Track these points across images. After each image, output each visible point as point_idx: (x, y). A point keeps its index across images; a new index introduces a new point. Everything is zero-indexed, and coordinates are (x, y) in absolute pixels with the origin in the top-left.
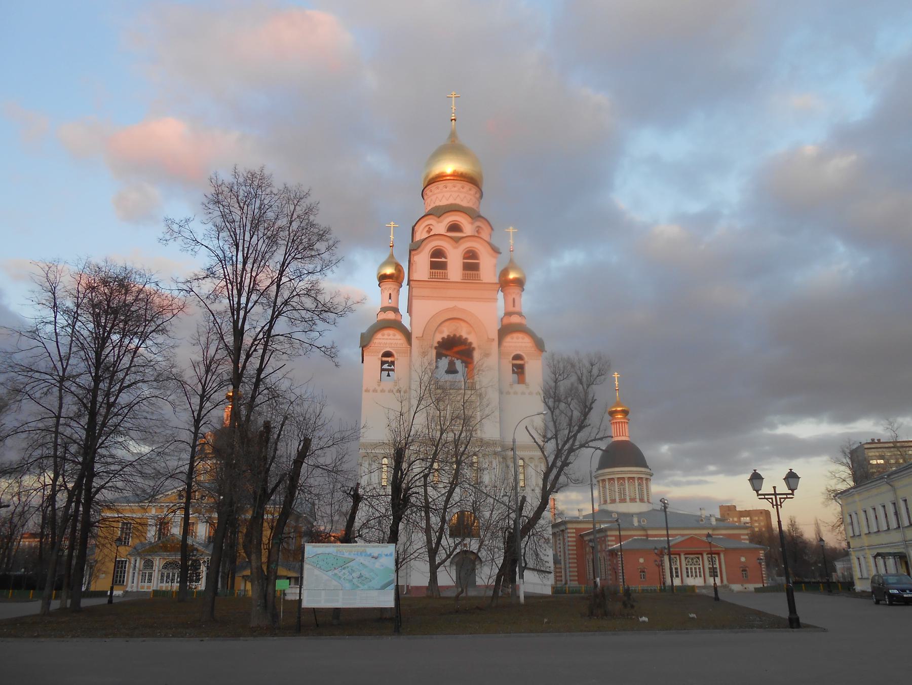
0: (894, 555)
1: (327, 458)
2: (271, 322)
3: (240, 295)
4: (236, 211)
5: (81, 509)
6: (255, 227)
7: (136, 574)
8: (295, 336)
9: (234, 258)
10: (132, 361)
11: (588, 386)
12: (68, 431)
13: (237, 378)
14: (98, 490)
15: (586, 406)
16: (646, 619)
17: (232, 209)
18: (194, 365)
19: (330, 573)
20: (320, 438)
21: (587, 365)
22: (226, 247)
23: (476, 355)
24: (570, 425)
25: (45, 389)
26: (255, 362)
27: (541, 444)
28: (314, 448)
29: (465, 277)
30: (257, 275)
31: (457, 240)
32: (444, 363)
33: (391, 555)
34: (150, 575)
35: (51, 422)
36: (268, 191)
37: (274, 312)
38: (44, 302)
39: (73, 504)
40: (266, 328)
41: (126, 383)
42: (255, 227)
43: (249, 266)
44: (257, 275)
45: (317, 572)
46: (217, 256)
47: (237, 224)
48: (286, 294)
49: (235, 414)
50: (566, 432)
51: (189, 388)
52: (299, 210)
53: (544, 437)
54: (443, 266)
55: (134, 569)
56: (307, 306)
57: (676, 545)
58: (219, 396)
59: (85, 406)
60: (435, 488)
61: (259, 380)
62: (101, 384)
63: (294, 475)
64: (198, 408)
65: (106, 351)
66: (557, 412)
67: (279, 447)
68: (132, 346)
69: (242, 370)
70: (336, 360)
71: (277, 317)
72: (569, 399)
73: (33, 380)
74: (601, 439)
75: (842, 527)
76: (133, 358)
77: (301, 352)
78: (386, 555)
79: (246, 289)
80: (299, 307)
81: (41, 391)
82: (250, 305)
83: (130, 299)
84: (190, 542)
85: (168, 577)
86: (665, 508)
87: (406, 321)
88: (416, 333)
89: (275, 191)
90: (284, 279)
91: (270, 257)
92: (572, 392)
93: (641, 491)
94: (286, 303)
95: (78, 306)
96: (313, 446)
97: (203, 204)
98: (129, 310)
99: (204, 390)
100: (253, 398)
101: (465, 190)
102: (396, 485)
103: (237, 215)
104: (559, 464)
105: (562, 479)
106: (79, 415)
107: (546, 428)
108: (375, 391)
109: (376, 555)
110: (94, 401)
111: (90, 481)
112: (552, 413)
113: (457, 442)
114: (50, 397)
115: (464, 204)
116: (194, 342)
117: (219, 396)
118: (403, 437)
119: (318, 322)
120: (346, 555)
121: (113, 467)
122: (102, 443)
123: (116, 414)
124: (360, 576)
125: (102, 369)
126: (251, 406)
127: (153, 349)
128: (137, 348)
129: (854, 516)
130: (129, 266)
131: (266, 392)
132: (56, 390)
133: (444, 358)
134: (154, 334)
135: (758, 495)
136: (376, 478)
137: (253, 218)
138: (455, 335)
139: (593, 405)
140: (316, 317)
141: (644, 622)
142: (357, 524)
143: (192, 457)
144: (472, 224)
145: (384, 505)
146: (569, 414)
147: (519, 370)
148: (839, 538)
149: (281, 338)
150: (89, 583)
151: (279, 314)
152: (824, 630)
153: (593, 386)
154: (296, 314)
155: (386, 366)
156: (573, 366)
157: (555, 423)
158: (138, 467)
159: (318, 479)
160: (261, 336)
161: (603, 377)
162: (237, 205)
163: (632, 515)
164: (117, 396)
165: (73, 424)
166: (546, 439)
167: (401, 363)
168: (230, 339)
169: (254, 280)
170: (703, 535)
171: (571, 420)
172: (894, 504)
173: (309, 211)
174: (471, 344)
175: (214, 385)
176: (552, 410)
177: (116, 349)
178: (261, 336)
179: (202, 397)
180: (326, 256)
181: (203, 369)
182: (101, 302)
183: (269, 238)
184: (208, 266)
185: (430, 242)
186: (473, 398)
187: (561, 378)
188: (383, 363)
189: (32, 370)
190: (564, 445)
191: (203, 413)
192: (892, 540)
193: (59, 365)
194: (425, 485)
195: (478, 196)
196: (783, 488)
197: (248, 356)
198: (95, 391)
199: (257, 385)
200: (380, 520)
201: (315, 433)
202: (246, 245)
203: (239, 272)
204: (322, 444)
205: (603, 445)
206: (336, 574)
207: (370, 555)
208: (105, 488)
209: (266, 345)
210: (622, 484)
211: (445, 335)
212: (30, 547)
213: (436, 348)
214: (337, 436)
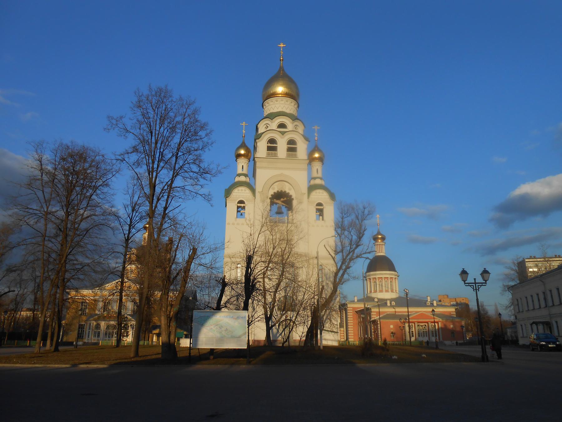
0: (543, 323)
1: (207, 259)
2: (172, 179)
3: (153, 163)
4: (150, 111)
7: (90, 333)
9: (150, 141)
12: (50, 245)
13: (151, 214)
14: (69, 280)
15: (360, 233)
16: (396, 357)
17: (148, 111)
20: (202, 248)
21: (361, 208)
22: (145, 134)
23: (295, 203)
24: (351, 244)
25: (36, 220)
26: (162, 203)
27: (334, 255)
28: (199, 254)
29: (288, 156)
30: (164, 151)
31: (283, 133)
36: (170, 99)
37: (174, 173)
38: (35, 167)
40: (169, 183)
41: (85, 215)
43: (159, 145)
44: (164, 151)
46: (140, 139)
47: (151, 120)
48: (181, 162)
49: (151, 235)
50: (349, 248)
51: (122, 220)
52: (189, 112)
53: (335, 251)
55: (90, 329)
56: (193, 170)
57: (412, 318)
58: (140, 225)
60: (270, 279)
61: (165, 215)
62: (70, 217)
63: (187, 270)
65: (73, 197)
66: (343, 236)
67: (177, 253)
68: (88, 194)
69: (155, 209)
70: (211, 202)
71: (176, 177)
72: (350, 229)
74: (369, 253)
75: (512, 307)
77: (190, 197)
79: (157, 159)
80: (188, 170)
81: (33, 221)
82: (159, 169)
83: (87, 165)
84: (123, 312)
85: (109, 334)
86: (407, 295)
89: (174, 100)
90: (180, 154)
91: (171, 140)
92: (352, 224)
93: (392, 285)
95: (55, 169)
96: (198, 253)
97: (130, 107)
98: (86, 173)
100: (162, 225)
101: (288, 103)
102: (248, 276)
103: (151, 114)
104: (344, 267)
105: (346, 276)
106: (56, 236)
107: (336, 245)
108: (233, 224)
112: (340, 237)
113: (283, 252)
114: (39, 224)
115: (288, 111)
116: (125, 193)
117: (140, 225)
118: (252, 248)
119: (200, 179)
123: (79, 235)
126: (160, 230)
127: (101, 196)
128: (91, 196)
129: (519, 300)
131: (169, 221)
133: (275, 205)
134: (101, 187)
136: (236, 273)
137: (161, 117)
138: (281, 191)
139: (365, 232)
140: (199, 176)
141: (395, 359)
142: (222, 303)
143: (124, 262)
144: (293, 123)
145: (240, 289)
146: (350, 238)
147: (320, 212)
148: (510, 314)
151: (177, 174)
153: (365, 221)
154: (187, 175)
156: (353, 209)
157: (342, 243)
159: (201, 272)
160: (166, 187)
161: (371, 216)
162: (151, 108)
163: (387, 300)
164: (79, 224)
165: (53, 240)
166: (336, 253)
167: (249, 207)
168: (147, 190)
169: (162, 154)
170: (429, 312)
171: (351, 241)
172: (544, 293)
173: (195, 112)
174: (291, 196)
175: (137, 219)
176: (340, 235)
178: (166, 187)
179: (130, 226)
180: (205, 140)
181: (130, 209)
182: (69, 167)
183: (170, 128)
184: (134, 145)
185: (268, 134)
186: (293, 228)
188: (238, 207)
189: (28, 208)
191: (130, 235)
192: (542, 315)
194: (264, 278)
195: (296, 106)
196: (480, 280)
197: (158, 200)
199: (163, 218)
200: (238, 296)
201: (199, 245)
202: (157, 132)
203: (153, 149)
204: (204, 251)
205: (371, 256)
209: (169, 193)
210: (380, 282)
211: (276, 191)
212: (27, 317)
213: (270, 198)
214: (213, 246)
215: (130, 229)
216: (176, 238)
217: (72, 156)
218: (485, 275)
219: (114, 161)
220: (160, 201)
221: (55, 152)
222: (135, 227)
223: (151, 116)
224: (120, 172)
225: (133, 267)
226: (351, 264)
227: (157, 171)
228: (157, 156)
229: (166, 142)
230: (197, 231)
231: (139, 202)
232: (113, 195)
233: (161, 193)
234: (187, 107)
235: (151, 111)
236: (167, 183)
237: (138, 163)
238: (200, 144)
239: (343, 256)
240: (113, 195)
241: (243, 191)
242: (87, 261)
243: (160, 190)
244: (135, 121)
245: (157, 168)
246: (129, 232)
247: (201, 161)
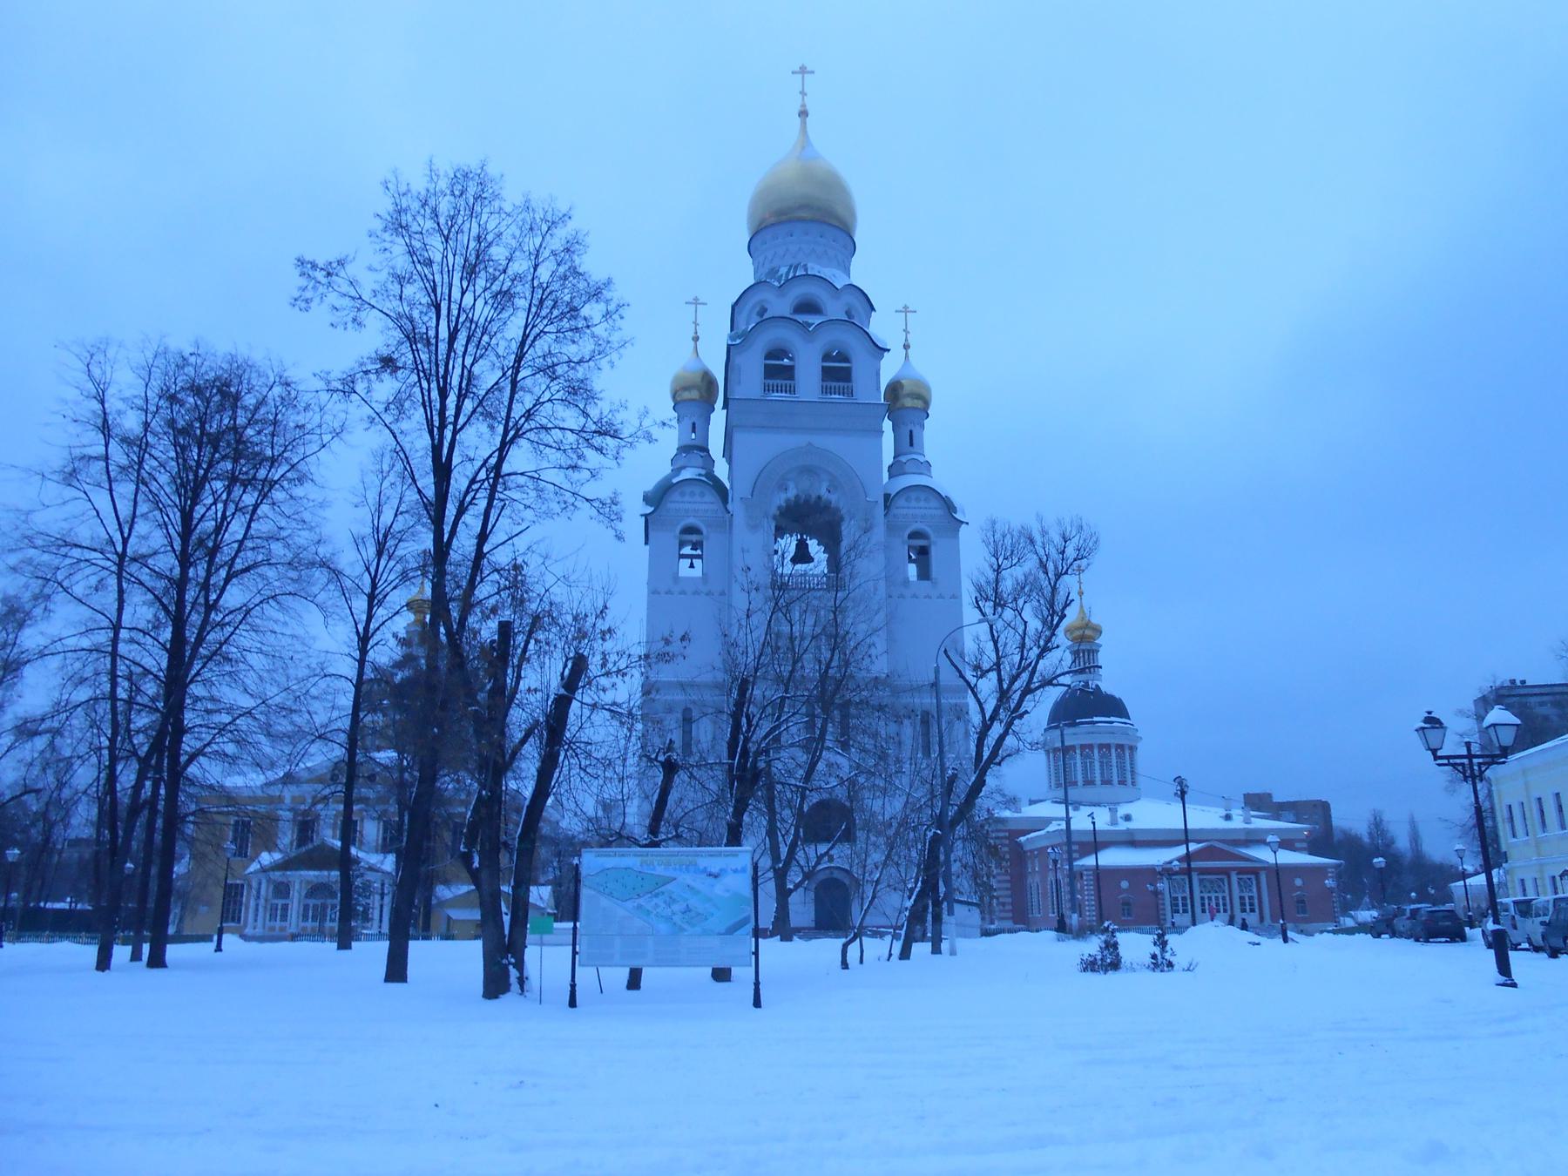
3: (443, 395)
5: (162, 792)
6: (470, 272)
7: (261, 909)
8: (545, 475)
10: (249, 527)
11: (1058, 576)
14: (192, 758)
18: (358, 542)
19: (630, 904)
22: (416, 314)
26: (472, 520)
32: (789, 544)
33: (744, 870)
34: (285, 908)
35: (103, 638)
36: (496, 204)
39: (148, 784)
40: (493, 461)
41: (238, 565)
42: (470, 272)
43: (459, 345)
45: (605, 902)
50: (1017, 658)
52: (556, 242)
54: (789, 373)
59: (165, 608)
64: (364, 617)
65: (199, 510)
70: (620, 526)
71: (512, 441)
72: (1021, 602)
73: (68, 561)
76: (251, 520)
78: (735, 871)
82: (462, 420)
87: (721, 470)
88: (739, 492)
89: (508, 208)
94: (528, 415)
99: (374, 586)
100: (472, 585)
105: (1010, 741)
109: (715, 870)
110: (180, 603)
111: (177, 741)
116: (356, 500)
117: (398, 598)
120: (660, 870)
121: (217, 718)
122: (198, 674)
123: (222, 625)
124: (688, 910)
125: (192, 545)
128: (256, 506)
130: (243, 352)
132: (112, 582)
135: (1436, 758)
145: (714, 781)
149: (522, 480)
150: (181, 920)
152: (757, 1003)
153: (1066, 577)
155: (687, 550)
157: (996, 643)
158: (263, 718)
160: (483, 475)
164: (223, 590)
168: (427, 483)
169: (469, 378)
174: (838, 510)
175: (392, 577)
177: (220, 506)
178: (483, 475)
179: (371, 597)
181: (372, 551)
187: (1006, 564)
190: (1012, 682)
191: (372, 626)
193: (117, 537)
198: (181, 584)
206: (639, 907)
207: (704, 870)
208: (204, 755)
211: (791, 493)
213: (774, 518)
215: (370, 607)
216: (521, 623)
217: (196, 390)
218: (1431, 734)
219: (324, 396)
220: (467, 518)
221: (145, 374)
222: (385, 604)
223: (437, 257)
224: (344, 435)
225: (379, 718)
226: (1027, 704)
227: (455, 423)
228: (455, 381)
229: (480, 335)
230: (587, 601)
231: (396, 527)
232: (322, 505)
233: (467, 492)
234: (544, 228)
235: (436, 242)
236: (486, 461)
237: (398, 404)
238: (586, 347)
239: (1000, 680)
240: (322, 505)
241: (697, 498)
242: (247, 702)
243: (466, 483)
244: (383, 276)
245: (457, 416)
246: (370, 617)
247: (591, 397)
